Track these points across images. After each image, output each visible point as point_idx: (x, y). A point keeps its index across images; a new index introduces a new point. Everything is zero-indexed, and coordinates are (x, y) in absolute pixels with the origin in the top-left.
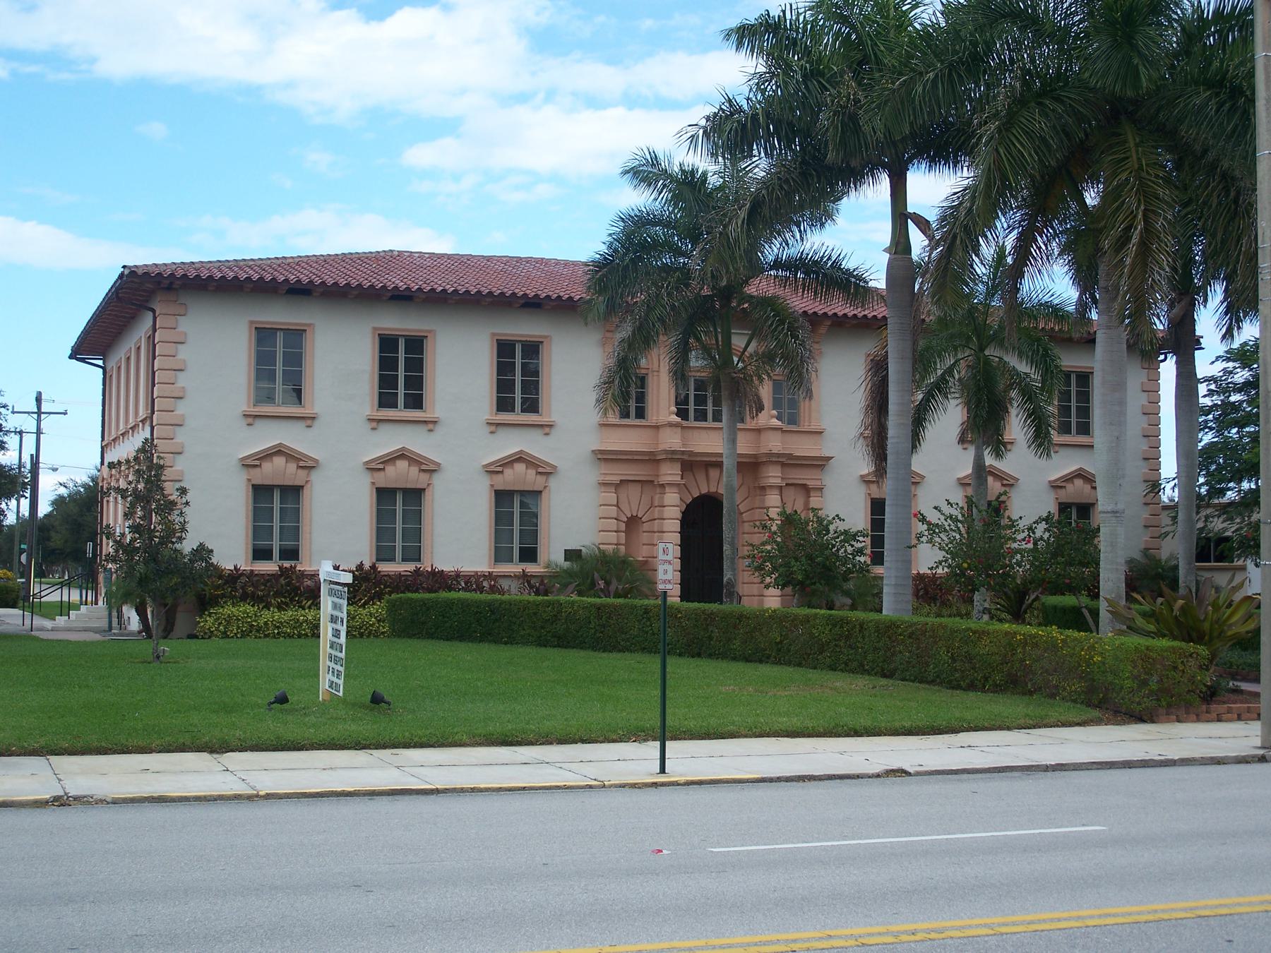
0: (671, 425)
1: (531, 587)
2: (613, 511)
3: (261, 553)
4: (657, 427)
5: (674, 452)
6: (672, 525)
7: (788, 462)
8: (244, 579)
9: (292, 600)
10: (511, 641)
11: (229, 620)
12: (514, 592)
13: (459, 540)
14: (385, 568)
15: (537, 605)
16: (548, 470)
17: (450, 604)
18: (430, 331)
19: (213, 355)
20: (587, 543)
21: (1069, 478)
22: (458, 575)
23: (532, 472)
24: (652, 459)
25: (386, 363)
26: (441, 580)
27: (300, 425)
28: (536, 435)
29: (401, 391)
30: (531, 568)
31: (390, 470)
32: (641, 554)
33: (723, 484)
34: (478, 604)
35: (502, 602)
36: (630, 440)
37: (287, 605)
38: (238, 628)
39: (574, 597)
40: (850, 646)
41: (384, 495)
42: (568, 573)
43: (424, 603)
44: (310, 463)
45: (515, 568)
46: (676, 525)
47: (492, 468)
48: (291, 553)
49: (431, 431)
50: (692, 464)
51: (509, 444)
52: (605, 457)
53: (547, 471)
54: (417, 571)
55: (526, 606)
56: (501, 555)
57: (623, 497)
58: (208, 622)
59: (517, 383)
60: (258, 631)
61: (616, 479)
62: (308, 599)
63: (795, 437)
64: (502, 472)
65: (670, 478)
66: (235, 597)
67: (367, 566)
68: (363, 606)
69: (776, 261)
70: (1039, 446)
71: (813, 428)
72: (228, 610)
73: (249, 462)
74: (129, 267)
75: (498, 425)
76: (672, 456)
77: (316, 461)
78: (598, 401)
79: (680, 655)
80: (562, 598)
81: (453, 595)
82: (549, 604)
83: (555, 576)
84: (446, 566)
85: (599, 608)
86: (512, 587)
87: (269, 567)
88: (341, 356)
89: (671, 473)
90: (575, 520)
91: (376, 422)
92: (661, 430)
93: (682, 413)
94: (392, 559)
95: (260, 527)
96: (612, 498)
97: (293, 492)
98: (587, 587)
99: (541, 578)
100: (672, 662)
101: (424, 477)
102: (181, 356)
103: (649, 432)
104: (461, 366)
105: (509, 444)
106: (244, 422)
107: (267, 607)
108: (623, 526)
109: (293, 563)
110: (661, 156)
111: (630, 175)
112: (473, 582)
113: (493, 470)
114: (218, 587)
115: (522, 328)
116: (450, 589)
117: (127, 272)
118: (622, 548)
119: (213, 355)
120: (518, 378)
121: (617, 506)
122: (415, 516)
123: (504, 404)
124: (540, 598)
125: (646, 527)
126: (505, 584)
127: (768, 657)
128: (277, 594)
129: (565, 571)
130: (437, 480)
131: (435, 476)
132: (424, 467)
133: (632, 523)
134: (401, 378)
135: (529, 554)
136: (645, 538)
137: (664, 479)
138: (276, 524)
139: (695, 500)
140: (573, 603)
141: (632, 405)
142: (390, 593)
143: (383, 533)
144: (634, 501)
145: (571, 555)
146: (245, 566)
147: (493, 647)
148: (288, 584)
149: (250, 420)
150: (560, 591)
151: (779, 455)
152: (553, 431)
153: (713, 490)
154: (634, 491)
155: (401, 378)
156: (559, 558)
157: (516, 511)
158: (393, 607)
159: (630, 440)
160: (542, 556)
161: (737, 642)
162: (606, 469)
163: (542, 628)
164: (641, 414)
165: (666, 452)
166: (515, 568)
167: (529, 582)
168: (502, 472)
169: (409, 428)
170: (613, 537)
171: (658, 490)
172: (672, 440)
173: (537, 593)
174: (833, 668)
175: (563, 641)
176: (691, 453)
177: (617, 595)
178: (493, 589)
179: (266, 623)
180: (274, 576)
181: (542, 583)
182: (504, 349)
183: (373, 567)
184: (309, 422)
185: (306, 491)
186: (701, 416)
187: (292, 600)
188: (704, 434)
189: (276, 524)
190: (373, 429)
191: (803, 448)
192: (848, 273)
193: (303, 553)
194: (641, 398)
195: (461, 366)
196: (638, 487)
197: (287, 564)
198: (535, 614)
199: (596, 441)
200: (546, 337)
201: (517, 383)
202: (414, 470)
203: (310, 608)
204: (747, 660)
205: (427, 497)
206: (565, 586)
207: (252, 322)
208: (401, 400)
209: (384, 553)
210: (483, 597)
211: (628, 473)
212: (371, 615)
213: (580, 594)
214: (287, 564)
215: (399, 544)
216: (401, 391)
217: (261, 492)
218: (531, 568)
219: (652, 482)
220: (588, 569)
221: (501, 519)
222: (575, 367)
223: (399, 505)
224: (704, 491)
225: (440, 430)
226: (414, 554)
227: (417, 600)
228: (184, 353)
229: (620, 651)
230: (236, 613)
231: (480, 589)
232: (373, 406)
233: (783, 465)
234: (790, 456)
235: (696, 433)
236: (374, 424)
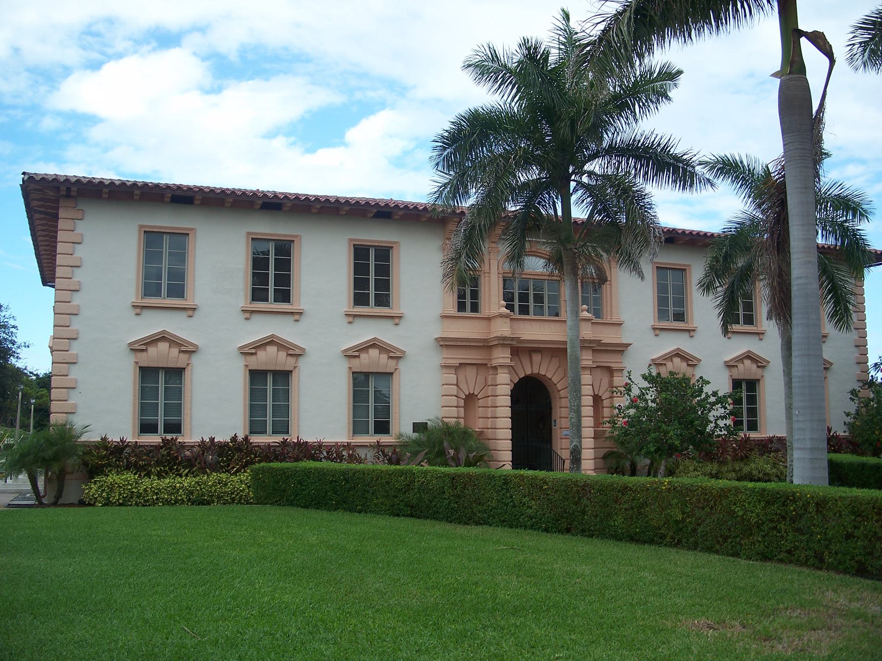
0: (501, 316)
1: (385, 455)
2: (453, 390)
3: (147, 428)
4: (489, 319)
5: (505, 338)
6: (504, 402)
7: (597, 347)
8: (127, 450)
9: (171, 469)
10: (364, 509)
11: (111, 488)
12: (371, 463)
13: (322, 415)
14: (256, 439)
15: (391, 474)
16: (398, 354)
17: (308, 472)
18: (297, 236)
19: (108, 250)
20: (432, 417)
21: (153, 341)
22: (320, 446)
23: (384, 357)
24: (486, 345)
25: (259, 263)
26: (306, 450)
27: (183, 315)
28: (387, 325)
29: (271, 287)
30: (385, 439)
31: (261, 354)
32: (478, 425)
33: (545, 368)
34: (333, 473)
35: (356, 472)
36: (467, 329)
37: (167, 473)
38: (120, 494)
39: (427, 467)
40: (799, 531)
41: (256, 376)
42: (417, 442)
43: (283, 471)
44: (191, 348)
45: (371, 439)
46: (507, 401)
47: (350, 353)
48: (175, 427)
49: (297, 321)
50: (520, 350)
51: (364, 332)
52: (445, 344)
53: (396, 355)
54: (284, 443)
55: (379, 475)
56: (358, 427)
57: (462, 377)
58: (93, 489)
59: (372, 280)
60: (138, 497)
61: (456, 362)
62: (185, 468)
63: (601, 328)
64: (358, 356)
65: (502, 361)
66: (118, 466)
67: (241, 437)
68: (235, 473)
69: (610, 145)
70: (839, 320)
71: (614, 320)
72: (113, 478)
73: (136, 347)
74: (28, 174)
75: (355, 316)
76: (503, 342)
77: (196, 346)
78: (444, 276)
79: (546, 530)
80: (414, 467)
81: (317, 464)
82: (402, 473)
83: (404, 445)
84: (309, 436)
85: (453, 478)
86: (370, 454)
87: (154, 439)
88: (219, 259)
89: (502, 357)
90: (422, 398)
91: (249, 313)
92: (493, 321)
93: (510, 307)
94: (264, 432)
95: (146, 407)
96: (452, 378)
97: (283, 377)
98: (438, 456)
99: (393, 446)
100: (58, 263)
101: (291, 360)
102: (78, 254)
103: (483, 323)
104: (323, 267)
105: (364, 332)
106: (132, 312)
107: (148, 475)
108: (462, 403)
109: (174, 436)
110: (500, 53)
111: (471, 68)
112: (334, 452)
113: (352, 354)
114: (102, 458)
115: (375, 235)
116: (314, 458)
117: (26, 178)
118: (462, 421)
119: (108, 250)
120: (372, 277)
121: (457, 385)
122: (283, 395)
123: (360, 299)
124: (393, 467)
125: (481, 403)
126: (362, 453)
127: (663, 537)
128: (158, 463)
129: (415, 441)
130: (302, 363)
131: (301, 359)
132: (291, 352)
133: (470, 399)
134: (271, 278)
135: (382, 427)
136: (480, 412)
137: (495, 363)
138: (161, 401)
139: (520, 379)
140: (426, 473)
141: (468, 301)
142: (260, 462)
143: (255, 409)
144: (471, 381)
145: (418, 427)
146: (130, 439)
147: (347, 516)
148: (169, 454)
149: (658, 332)
150: (410, 461)
151: (591, 341)
152: (402, 322)
153: (536, 371)
154: (471, 373)
155: (271, 278)
156: (407, 430)
157: (370, 392)
158: (255, 475)
159: (467, 329)
160: (394, 428)
161: (620, 519)
162: (447, 353)
163: (395, 497)
164: (475, 308)
165: (498, 338)
166: (371, 439)
167: (383, 452)
168: (358, 356)
169: (280, 318)
170: (454, 412)
171: (491, 372)
172: (502, 328)
173: (390, 462)
174: (765, 557)
175: (416, 511)
176: (518, 339)
177: (469, 464)
178: (352, 458)
179: (145, 490)
180: (157, 448)
181: (394, 452)
182: (360, 253)
183: (246, 439)
184: (190, 313)
185: (187, 373)
186: (524, 310)
187: (171, 469)
188: (527, 325)
189: (161, 401)
190: (247, 319)
191: (608, 336)
192: (677, 159)
193: (185, 428)
194: (475, 295)
195: (323, 267)
196: (475, 368)
197: (169, 437)
198: (388, 483)
199: (438, 331)
200: (395, 243)
201: (372, 280)
202: (282, 355)
203: (187, 475)
204: (633, 539)
205: (294, 377)
206: (415, 454)
207: (141, 226)
208: (164, 291)
209: (256, 427)
210: (344, 465)
211: (466, 357)
212: (241, 481)
213: (430, 463)
214: (169, 437)
215: (269, 419)
216: (271, 287)
217: (147, 373)
218: (385, 439)
219: (486, 364)
220: (436, 441)
221: (359, 395)
222: (420, 273)
223: (270, 386)
224: (529, 372)
225: (304, 321)
226: (282, 427)
227: (278, 469)
228: (80, 252)
229: (477, 523)
230: (118, 481)
231: (340, 458)
232: (246, 298)
233: (594, 351)
234: (599, 342)
235: (521, 324)
236: (247, 315)
